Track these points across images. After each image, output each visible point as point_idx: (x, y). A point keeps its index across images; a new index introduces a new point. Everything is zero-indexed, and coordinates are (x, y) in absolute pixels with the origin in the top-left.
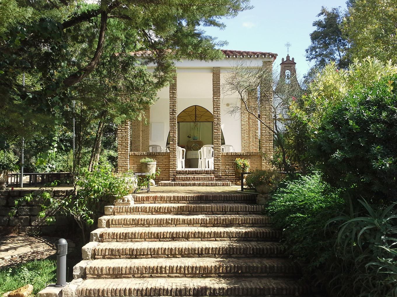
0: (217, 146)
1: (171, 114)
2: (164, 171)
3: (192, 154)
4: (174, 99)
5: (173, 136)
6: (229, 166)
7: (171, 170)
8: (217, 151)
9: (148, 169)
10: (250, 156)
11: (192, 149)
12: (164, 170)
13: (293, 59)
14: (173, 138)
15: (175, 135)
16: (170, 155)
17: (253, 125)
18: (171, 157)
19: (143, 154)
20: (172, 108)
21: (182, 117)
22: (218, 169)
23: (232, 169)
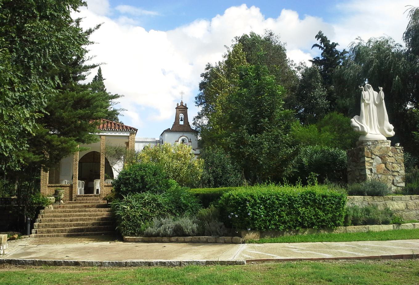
13: (186, 104)
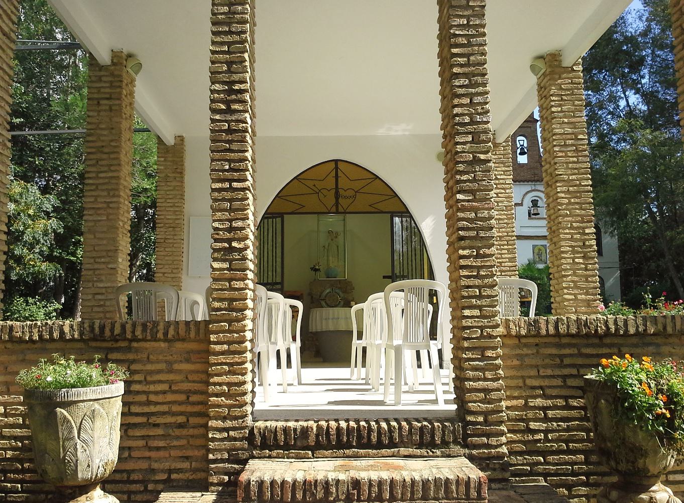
0: (477, 282)
1: (220, 112)
2: (178, 432)
3: (328, 319)
4: (236, 27)
5: (231, 229)
6: (545, 396)
7: (219, 424)
8: (476, 312)
9: (62, 432)
10: (659, 340)
11: (323, 303)
12: (181, 426)
14: (229, 241)
15: (239, 224)
16: (213, 338)
17: (570, 203)
18: (218, 348)
19: (56, 335)
20: (224, 77)
21: (292, 199)
22: (486, 414)
23: (565, 413)
